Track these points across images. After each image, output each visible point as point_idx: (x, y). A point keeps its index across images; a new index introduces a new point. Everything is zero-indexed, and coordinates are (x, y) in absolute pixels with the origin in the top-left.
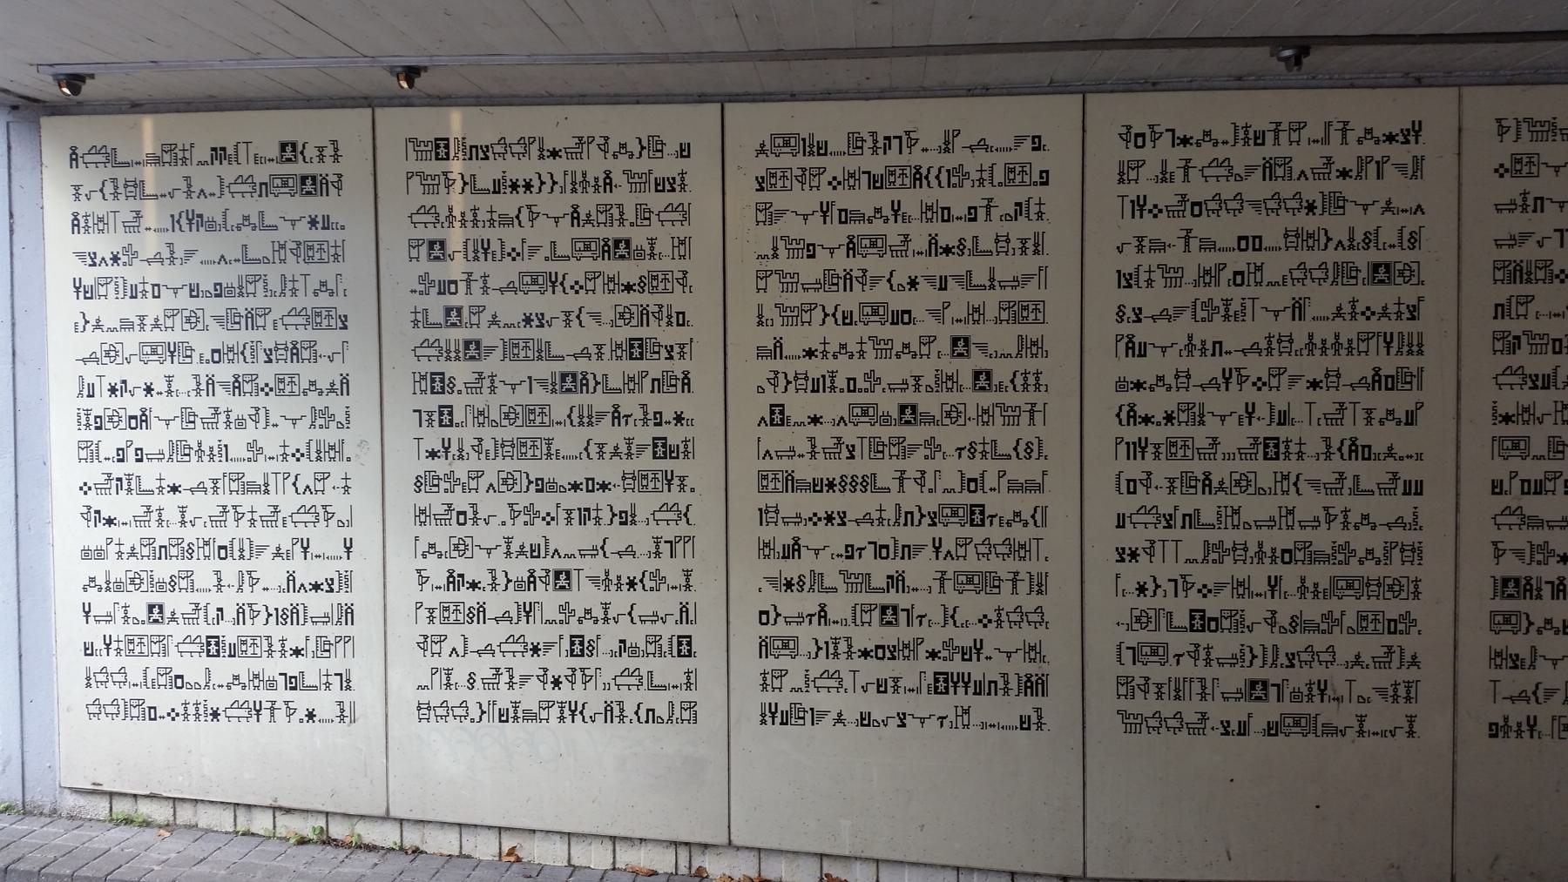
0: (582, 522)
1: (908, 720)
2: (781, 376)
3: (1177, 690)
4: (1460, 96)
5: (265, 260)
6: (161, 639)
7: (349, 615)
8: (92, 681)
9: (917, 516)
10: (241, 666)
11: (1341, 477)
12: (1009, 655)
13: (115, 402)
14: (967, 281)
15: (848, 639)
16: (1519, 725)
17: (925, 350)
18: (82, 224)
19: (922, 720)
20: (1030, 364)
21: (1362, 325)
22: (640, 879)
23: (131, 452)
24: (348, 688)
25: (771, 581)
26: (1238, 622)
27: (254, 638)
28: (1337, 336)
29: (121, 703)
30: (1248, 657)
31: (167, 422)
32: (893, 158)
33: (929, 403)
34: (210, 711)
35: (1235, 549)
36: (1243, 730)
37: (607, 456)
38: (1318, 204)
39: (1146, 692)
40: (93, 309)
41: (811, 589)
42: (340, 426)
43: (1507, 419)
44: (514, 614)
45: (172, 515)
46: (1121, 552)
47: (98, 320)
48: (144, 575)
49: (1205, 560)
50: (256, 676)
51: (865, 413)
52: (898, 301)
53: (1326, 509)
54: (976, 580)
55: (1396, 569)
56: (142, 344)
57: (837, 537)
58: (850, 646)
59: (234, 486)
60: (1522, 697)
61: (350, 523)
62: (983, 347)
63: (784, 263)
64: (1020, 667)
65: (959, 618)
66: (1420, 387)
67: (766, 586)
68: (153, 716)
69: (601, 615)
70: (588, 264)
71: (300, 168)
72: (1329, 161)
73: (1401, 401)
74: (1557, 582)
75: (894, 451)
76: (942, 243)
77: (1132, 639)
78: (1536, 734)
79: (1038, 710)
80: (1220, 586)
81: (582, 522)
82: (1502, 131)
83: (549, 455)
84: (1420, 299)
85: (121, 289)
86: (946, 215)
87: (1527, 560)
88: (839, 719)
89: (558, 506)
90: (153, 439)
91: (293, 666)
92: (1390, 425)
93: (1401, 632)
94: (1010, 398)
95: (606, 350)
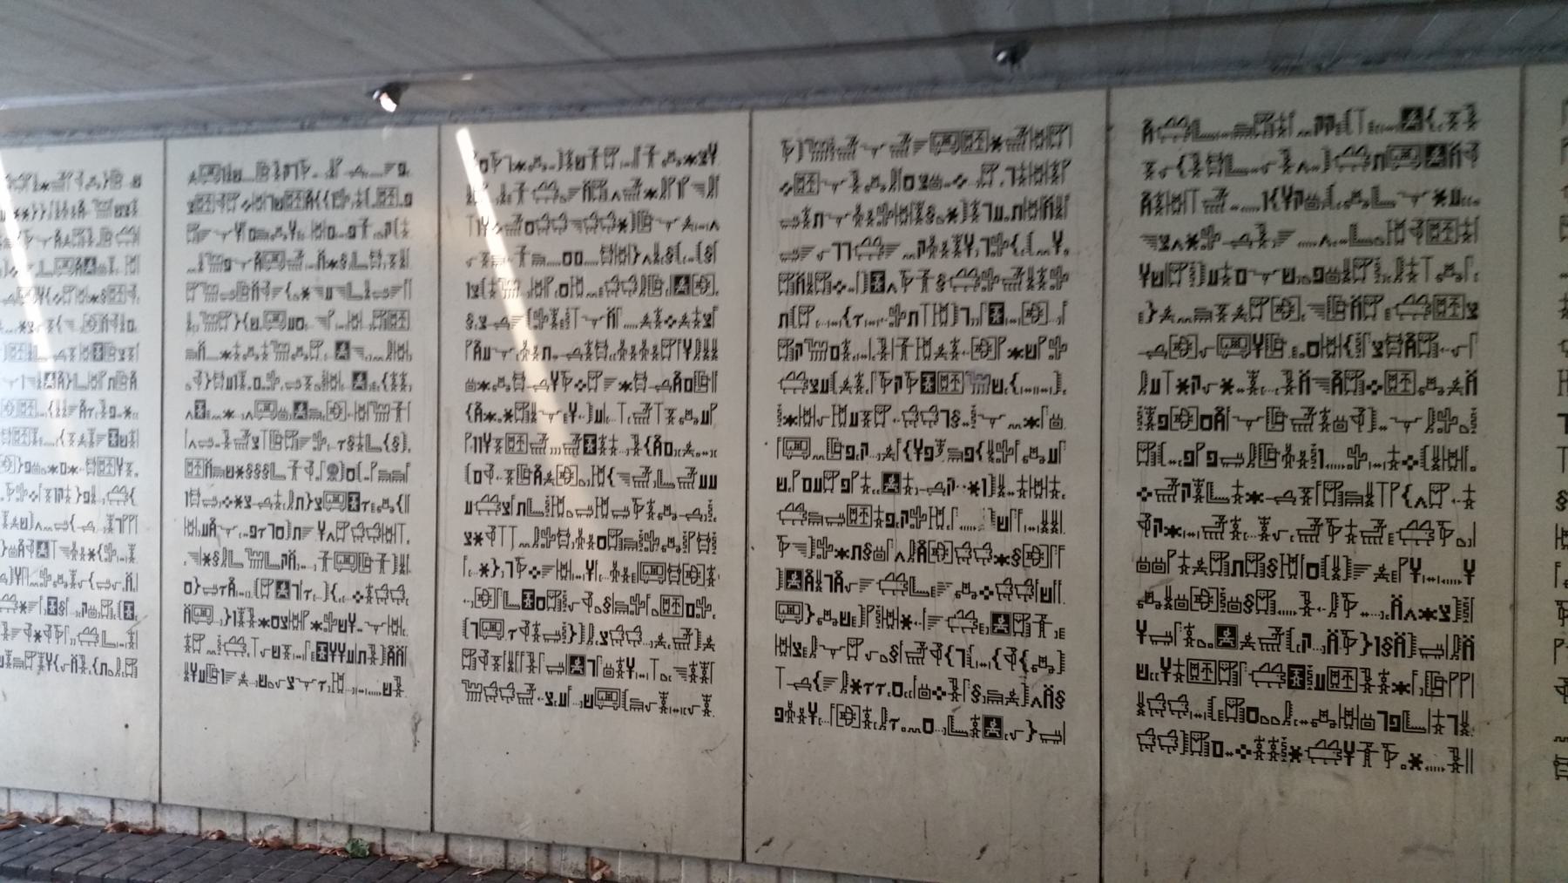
0: (58, 499)
1: (296, 683)
2: (204, 375)
3: (511, 663)
4: (1523, 79)
5: (1378, 241)
6: (1231, 666)
7: (1469, 649)
8: (1146, 709)
9: (306, 502)
10: (1331, 701)
11: (647, 470)
12: (376, 628)
13: (1186, 400)
14: (347, 291)
15: (251, 609)
16: (802, 710)
17: (314, 353)
18: (1154, 204)
19: (307, 684)
20: (395, 366)
21: (665, 332)
22: (717, 874)
23: (1202, 456)
24: (1465, 733)
25: (194, 555)
26: (563, 604)
27: (1348, 669)
28: (644, 343)
29: (1180, 735)
30: (569, 634)
31: (1249, 423)
32: (290, 183)
33: (317, 400)
34: (1289, 750)
35: (559, 535)
36: (564, 702)
37: (76, 443)
38: (629, 222)
39: (485, 664)
40: (1162, 297)
41: (224, 564)
42: (1464, 430)
43: (790, 420)
44: (8, 576)
45: (1251, 525)
46: (468, 536)
47: (1168, 310)
48: (1213, 593)
49: (536, 544)
50: (1349, 713)
51: (267, 409)
52: (295, 309)
53: (635, 500)
54: (352, 559)
55: (693, 558)
56: (1220, 337)
57: (244, 518)
58: (252, 616)
59: (1330, 496)
60: (804, 684)
61: (1473, 543)
62: (360, 350)
63: (207, 276)
64: (384, 639)
65: (338, 595)
66: (714, 389)
67: (191, 562)
68: (1218, 752)
69: (70, 581)
70: (67, 279)
71: (1425, 137)
72: (638, 183)
73: (697, 402)
74: (835, 576)
75: (290, 442)
76: (329, 258)
77: (476, 615)
78: (816, 720)
79: (397, 678)
80: (547, 568)
81: (58, 499)
82: (787, 152)
83: (35, 442)
84: (715, 308)
85: (1198, 274)
86: (332, 233)
87: (809, 554)
88: (243, 680)
89: (40, 486)
90: (1228, 442)
91: (1395, 704)
92: (689, 424)
93: (698, 616)
94: (383, 397)
95: (77, 352)
